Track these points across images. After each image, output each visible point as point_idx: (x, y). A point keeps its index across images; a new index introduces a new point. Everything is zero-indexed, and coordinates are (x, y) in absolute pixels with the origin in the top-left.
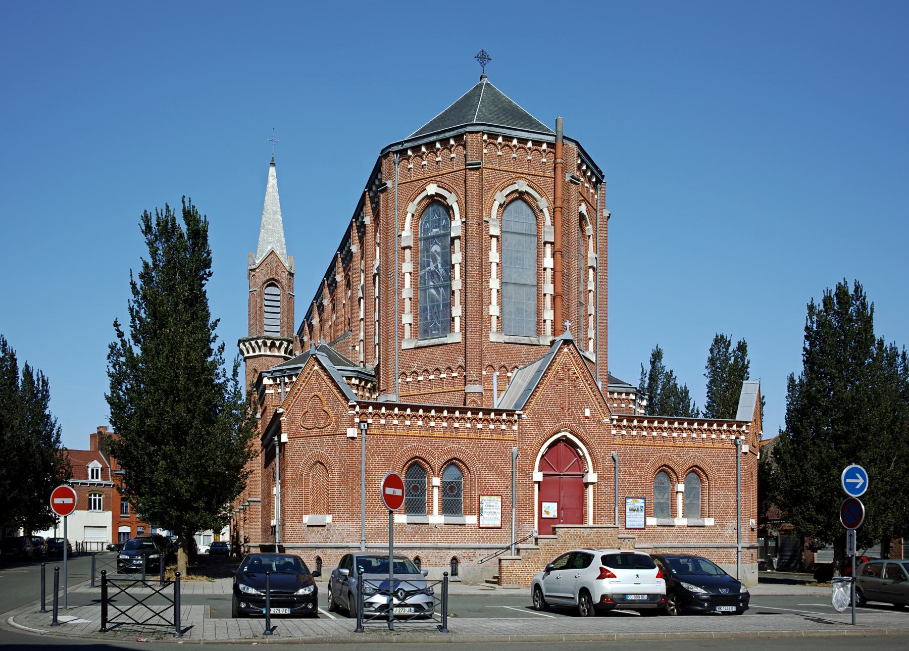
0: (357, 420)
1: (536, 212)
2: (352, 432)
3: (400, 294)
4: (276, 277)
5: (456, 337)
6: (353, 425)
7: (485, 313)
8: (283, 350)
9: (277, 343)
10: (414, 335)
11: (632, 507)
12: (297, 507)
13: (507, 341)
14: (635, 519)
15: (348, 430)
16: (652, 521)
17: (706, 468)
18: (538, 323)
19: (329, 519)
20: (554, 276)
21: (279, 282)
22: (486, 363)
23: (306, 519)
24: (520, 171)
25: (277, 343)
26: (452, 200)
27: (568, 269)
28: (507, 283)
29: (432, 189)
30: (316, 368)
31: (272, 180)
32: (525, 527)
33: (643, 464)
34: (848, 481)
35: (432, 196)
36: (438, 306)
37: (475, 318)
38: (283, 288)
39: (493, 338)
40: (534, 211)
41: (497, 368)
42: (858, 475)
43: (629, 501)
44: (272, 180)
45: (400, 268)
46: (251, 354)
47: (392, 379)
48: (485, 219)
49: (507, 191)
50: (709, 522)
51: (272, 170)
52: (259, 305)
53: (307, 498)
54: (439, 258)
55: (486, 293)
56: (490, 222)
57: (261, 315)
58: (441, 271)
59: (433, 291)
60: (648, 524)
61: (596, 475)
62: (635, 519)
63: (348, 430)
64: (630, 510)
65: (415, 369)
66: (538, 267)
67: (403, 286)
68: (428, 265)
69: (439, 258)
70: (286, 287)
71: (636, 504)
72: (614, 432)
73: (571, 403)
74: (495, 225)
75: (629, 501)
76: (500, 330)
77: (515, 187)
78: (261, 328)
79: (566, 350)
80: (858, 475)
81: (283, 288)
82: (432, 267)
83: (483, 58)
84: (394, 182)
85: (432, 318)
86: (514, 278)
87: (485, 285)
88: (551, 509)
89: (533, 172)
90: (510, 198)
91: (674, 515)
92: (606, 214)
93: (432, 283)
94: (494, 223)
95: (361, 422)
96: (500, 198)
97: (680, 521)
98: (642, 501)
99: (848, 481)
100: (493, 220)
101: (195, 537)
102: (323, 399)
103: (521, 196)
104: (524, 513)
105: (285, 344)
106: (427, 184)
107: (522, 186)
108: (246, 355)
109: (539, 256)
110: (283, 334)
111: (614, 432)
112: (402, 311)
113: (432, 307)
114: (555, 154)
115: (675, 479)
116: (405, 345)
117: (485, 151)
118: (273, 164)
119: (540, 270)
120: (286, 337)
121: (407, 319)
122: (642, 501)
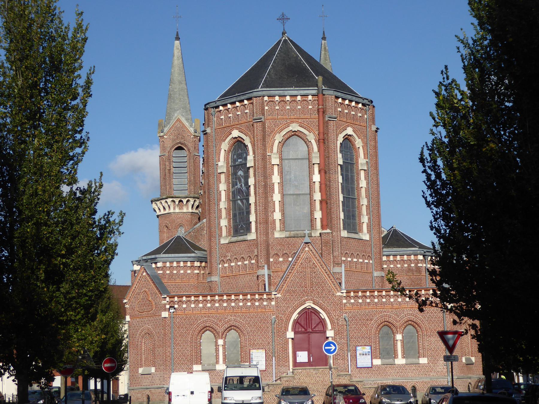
0: (168, 306)
1: (307, 142)
2: (165, 314)
3: (218, 205)
4: (182, 141)
5: (252, 236)
6: (165, 310)
7: (270, 218)
8: (190, 206)
9: (185, 201)
10: (229, 234)
11: (361, 352)
12: (136, 362)
13: (288, 236)
14: (364, 361)
15: (163, 313)
16: (377, 362)
17: (419, 322)
18: (311, 220)
19: (153, 370)
20: (320, 187)
21: (186, 146)
22: (272, 253)
23: (141, 370)
24: (292, 117)
25: (185, 201)
26: (247, 142)
27: (330, 182)
28: (287, 195)
29: (235, 133)
30: (144, 274)
31: (177, 53)
32: (283, 369)
33: (368, 322)
34: (326, 348)
35: (236, 138)
36: (243, 213)
37: (266, 223)
38: (189, 150)
39: (277, 235)
40: (306, 142)
41: (281, 256)
42: (332, 345)
43: (358, 348)
44: (177, 53)
45: (218, 187)
46: (163, 212)
47: (214, 265)
48: (268, 154)
49: (284, 132)
50: (423, 361)
51: (177, 43)
52: (168, 168)
53: (141, 357)
54: (243, 180)
55: (271, 205)
56: (272, 156)
57: (170, 177)
58: (244, 188)
59: (239, 202)
60: (374, 364)
61: (333, 331)
62: (364, 361)
63: (163, 313)
64: (360, 354)
65: (229, 258)
66: (310, 182)
67: (220, 200)
68: (237, 185)
69: (243, 180)
70: (192, 149)
71: (365, 350)
72: (344, 301)
73: (312, 284)
74: (275, 158)
75: (358, 348)
76: (283, 228)
77: (290, 128)
78: (170, 188)
79: (307, 249)
80: (332, 345)
81: (189, 150)
82: (239, 186)
83: (283, 19)
84: (212, 128)
85: (240, 222)
86: (291, 191)
87: (270, 199)
88: (303, 357)
89: (302, 116)
90: (286, 137)
91: (396, 356)
92: (374, 128)
93: (239, 197)
94: (275, 156)
95: (170, 307)
96: (278, 138)
97: (400, 361)
98: (369, 348)
99: (326, 348)
100: (274, 154)
101: (483, 377)
102: (149, 293)
103: (295, 134)
104: (282, 360)
105: (192, 200)
106: (232, 130)
107: (295, 127)
108: (158, 213)
109: (311, 173)
110: (190, 192)
111: (344, 301)
112: (220, 217)
113: (240, 213)
114: (318, 100)
115: (394, 329)
116: (223, 241)
117: (266, 108)
118: (178, 38)
119: (312, 183)
120: (192, 195)
121: (224, 223)
122: (369, 348)
